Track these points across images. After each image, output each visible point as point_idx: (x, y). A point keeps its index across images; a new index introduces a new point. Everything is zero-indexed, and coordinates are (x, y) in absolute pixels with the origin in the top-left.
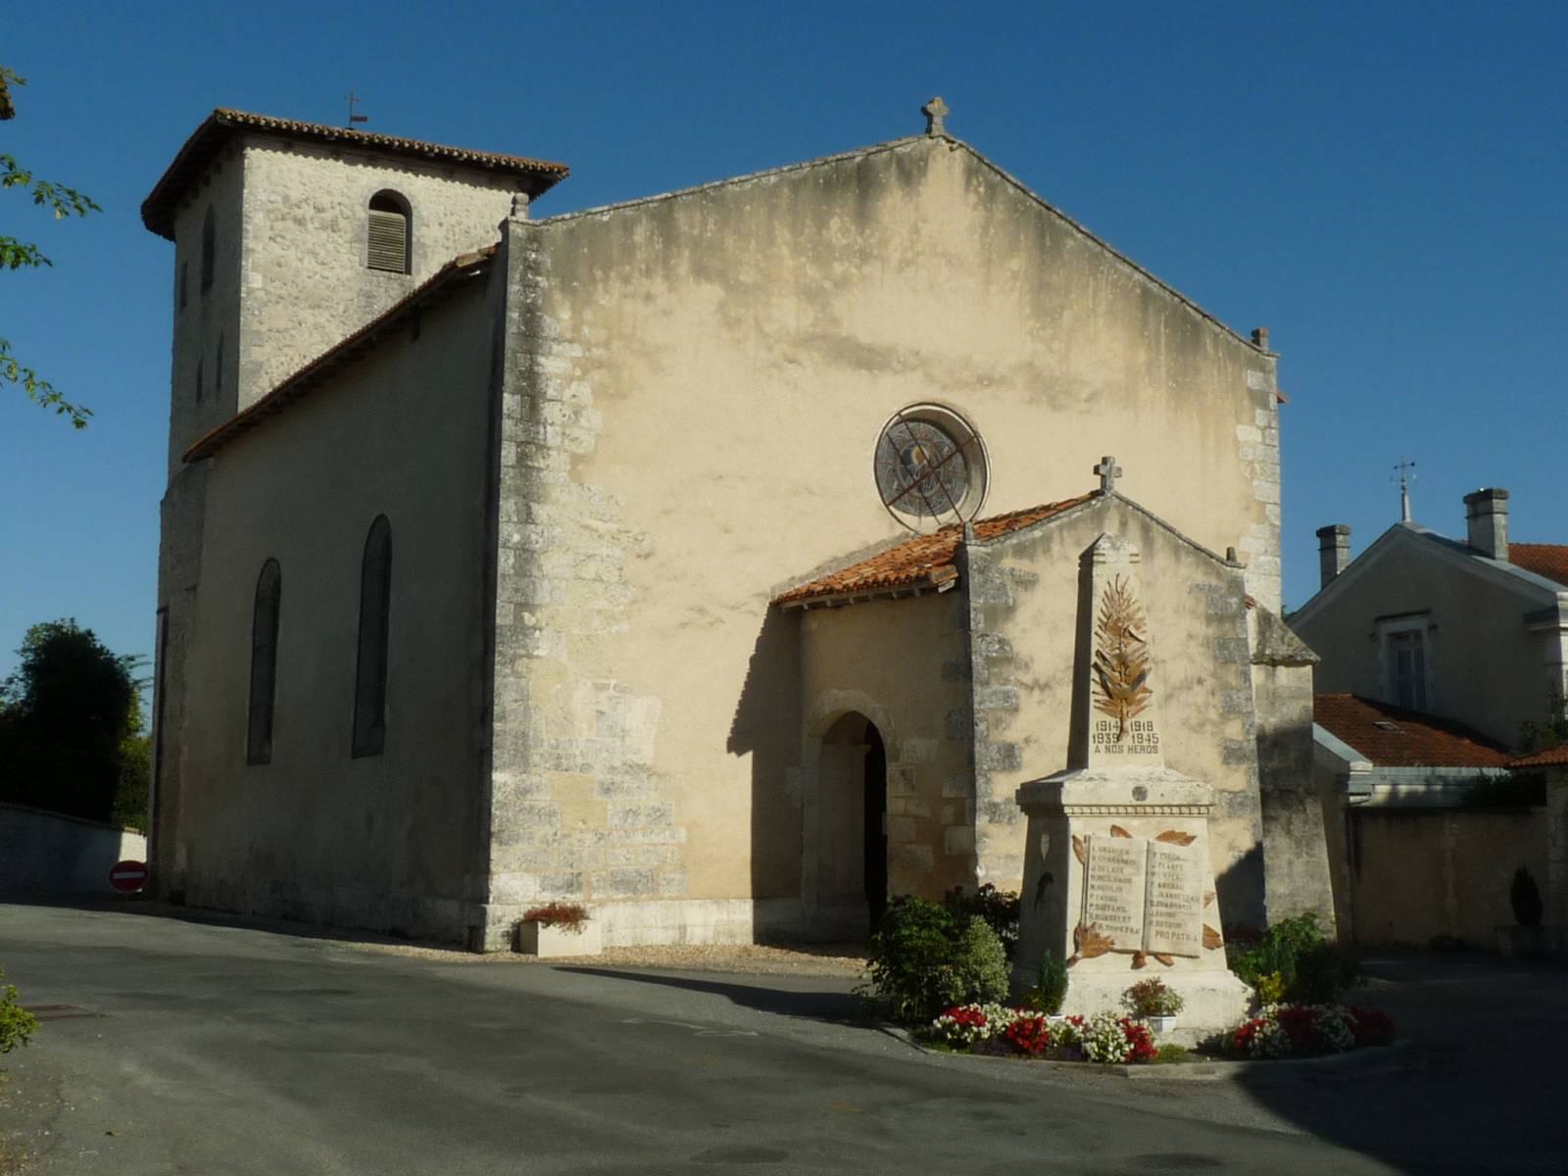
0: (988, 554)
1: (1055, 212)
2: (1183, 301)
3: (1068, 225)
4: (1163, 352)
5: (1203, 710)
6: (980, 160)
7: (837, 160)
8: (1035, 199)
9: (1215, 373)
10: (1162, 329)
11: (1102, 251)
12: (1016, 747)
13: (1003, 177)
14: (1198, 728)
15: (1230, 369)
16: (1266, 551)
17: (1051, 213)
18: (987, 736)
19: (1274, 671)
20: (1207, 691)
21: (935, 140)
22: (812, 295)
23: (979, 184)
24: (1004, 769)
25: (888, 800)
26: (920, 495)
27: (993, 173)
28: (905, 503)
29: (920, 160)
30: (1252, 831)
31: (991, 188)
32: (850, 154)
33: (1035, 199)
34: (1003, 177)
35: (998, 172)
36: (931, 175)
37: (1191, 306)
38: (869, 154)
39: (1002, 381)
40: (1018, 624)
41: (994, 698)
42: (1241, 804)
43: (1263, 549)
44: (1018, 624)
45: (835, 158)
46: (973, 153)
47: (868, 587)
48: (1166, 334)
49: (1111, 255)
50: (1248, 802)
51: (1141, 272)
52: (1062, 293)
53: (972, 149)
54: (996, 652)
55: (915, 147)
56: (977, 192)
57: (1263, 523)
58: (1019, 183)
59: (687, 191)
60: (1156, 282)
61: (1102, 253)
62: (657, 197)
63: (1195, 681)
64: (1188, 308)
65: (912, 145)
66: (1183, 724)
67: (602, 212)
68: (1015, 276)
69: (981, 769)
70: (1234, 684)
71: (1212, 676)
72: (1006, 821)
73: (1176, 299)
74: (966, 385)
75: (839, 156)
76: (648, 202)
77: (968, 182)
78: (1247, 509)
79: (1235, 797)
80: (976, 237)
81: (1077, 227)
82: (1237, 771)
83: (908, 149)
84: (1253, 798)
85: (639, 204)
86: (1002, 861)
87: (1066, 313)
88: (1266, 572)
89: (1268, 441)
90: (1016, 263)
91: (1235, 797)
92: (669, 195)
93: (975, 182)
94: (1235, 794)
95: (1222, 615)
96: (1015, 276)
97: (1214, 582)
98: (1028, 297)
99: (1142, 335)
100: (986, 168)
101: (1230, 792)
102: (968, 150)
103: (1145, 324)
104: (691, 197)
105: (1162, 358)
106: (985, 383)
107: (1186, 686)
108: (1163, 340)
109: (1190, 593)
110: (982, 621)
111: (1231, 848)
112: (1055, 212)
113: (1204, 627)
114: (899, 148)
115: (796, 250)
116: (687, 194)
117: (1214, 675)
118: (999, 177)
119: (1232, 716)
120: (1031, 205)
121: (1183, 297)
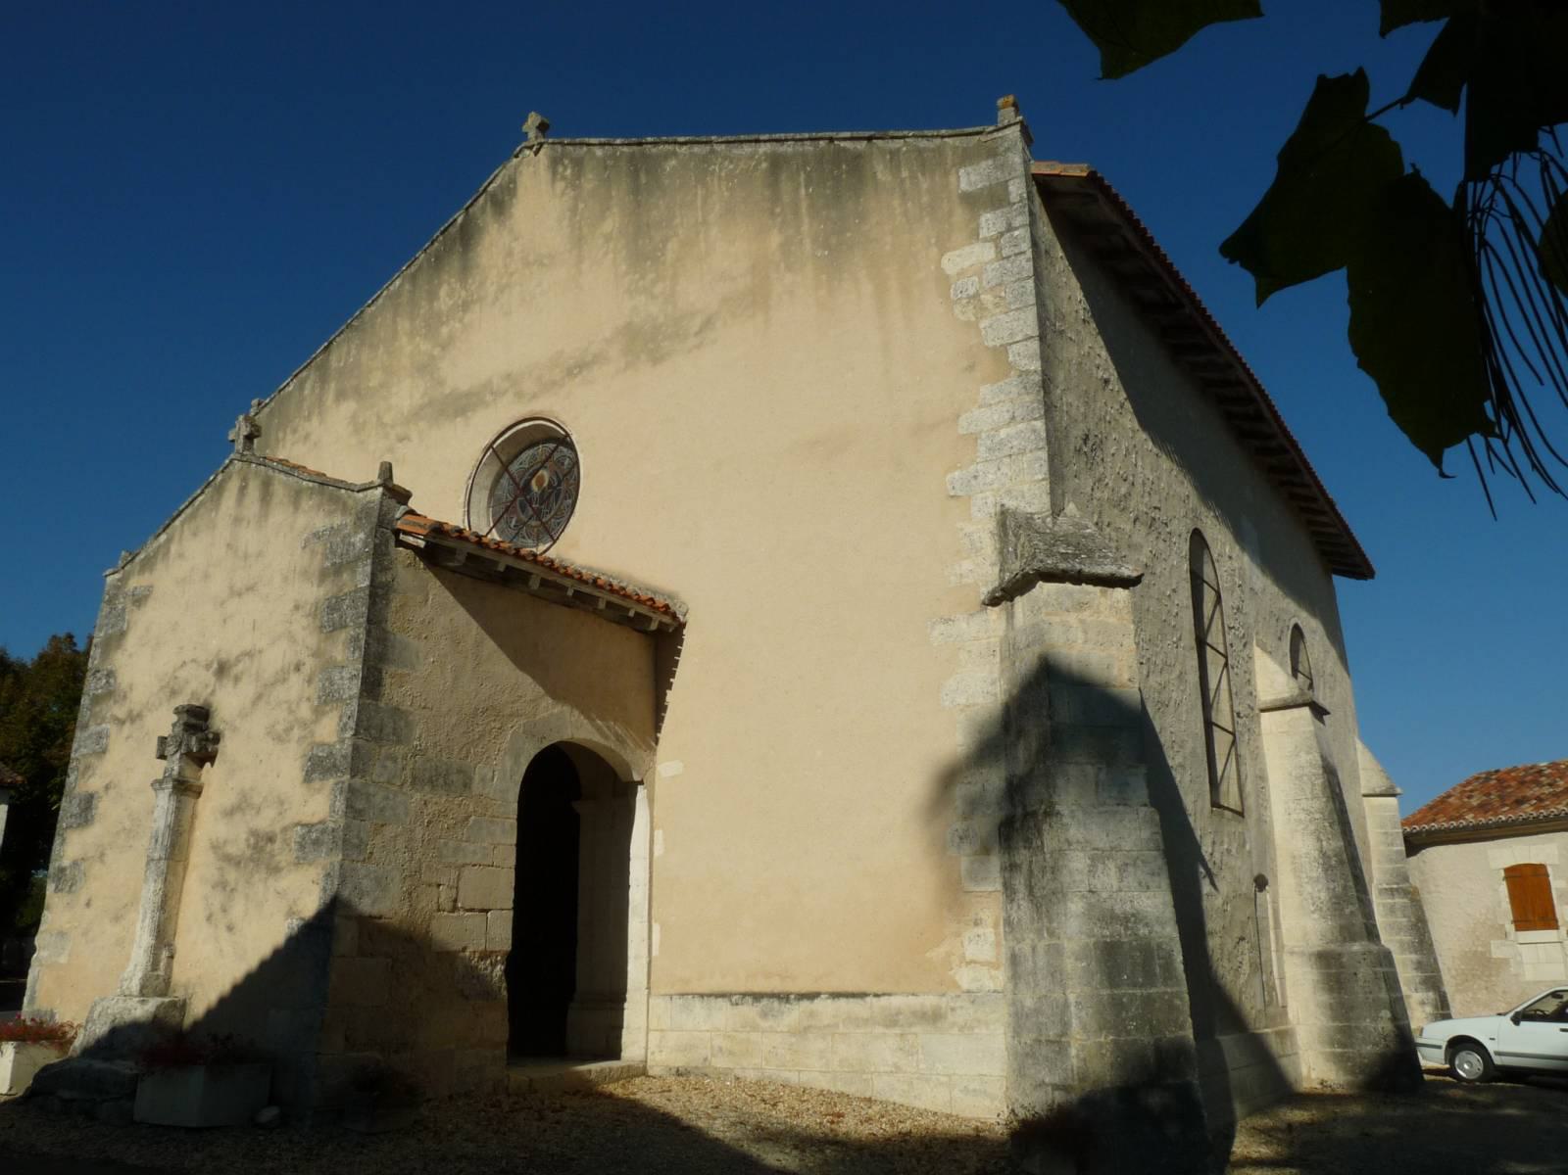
0: (119, 580)
1: (647, 143)
2: (831, 140)
3: (667, 146)
4: (806, 220)
5: (294, 707)
6: (562, 144)
7: (442, 233)
8: (622, 145)
9: (896, 203)
10: (803, 191)
11: (905, 142)
12: (96, 796)
13: (588, 145)
14: (280, 739)
15: (925, 186)
16: (1013, 418)
17: (644, 146)
18: (74, 788)
19: (1012, 606)
20: (304, 680)
21: (521, 156)
22: (426, 368)
23: (565, 168)
24: (79, 825)
25: (512, 861)
26: (539, 523)
27: (578, 148)
28: (524, 537)
29: (510, 183)
30: (322, 884)
31: (578, 164)
32: (451, 220)
33: (622, 145)
34: (588, 145)
35: (581, 144)
36: (521, 191)
37: (845, 139)
38: (467, 209)
39: (598, 359)
40: (126, 650)
41: (89, 742)
42: (316, 843)
43: (1007, 416)
44: (126, 650)
45: (438, 233)
46: (553, 143)
47: (1140, 622)
48: (807, 194)
49: (723, 146)
50: (327, 838)
51: (765, 141)
52: (664, 224)
53: (550, 140)
54: (102, 688)
55: (504, 175)
56: (564, 178)
57: (1007, 376)
58: (603, 140)
59: (337, 333)
60: (787, 140)
61: (712, 152)
62: (319, 351)
63: (292, 668)
64: (842, 144)
65: (501, 175)
66: (268, 733)
67: (288, 384)
68: (608, 238)
69: (61, 826)
70: (339, 658)
71: (313, 656)
72: (67, 888)
73: (822, 143)
74: (554, 383)
75: (442, 229)
76: (315, 358)
77: (554, 173)
78: (971, 368)
79: (310, 831)
80: (566, 223)
81: (675, 143)
82: (319, 791)
83: (498, 181)
84: (333, 830)
85: (309, 364)
86: (53, 938)
87: (670, 246)
88: (1015, 450)
89: (1005, 252)
90: (611, 224)
91: (310, 831)
92: (326, 344)
93: (560, 169)
94: (309, 826)
95: (341, 564)
96: (608, 238)
97: (337, 520)
98: (624, 253)
99: (772, 213)
100: (570, 148)
101: (303, 825)
102: (549, 144)
103: (776, 198)
104: (342, 336)
105: (805, 228)
106: (575, 372)
107: (282, 678)
108: (804, 206)
109: (304, 547)
110: (98, 656)
111: (290, 913)
112: (647, 143)
113: (315, 589)
114: (492, 186)
115: (412, 335)
116: (339, 335)
117: (316, 654)
118: (585, 148)
119: (328, 708)
120: (622, 153)
121: (828, 134)
